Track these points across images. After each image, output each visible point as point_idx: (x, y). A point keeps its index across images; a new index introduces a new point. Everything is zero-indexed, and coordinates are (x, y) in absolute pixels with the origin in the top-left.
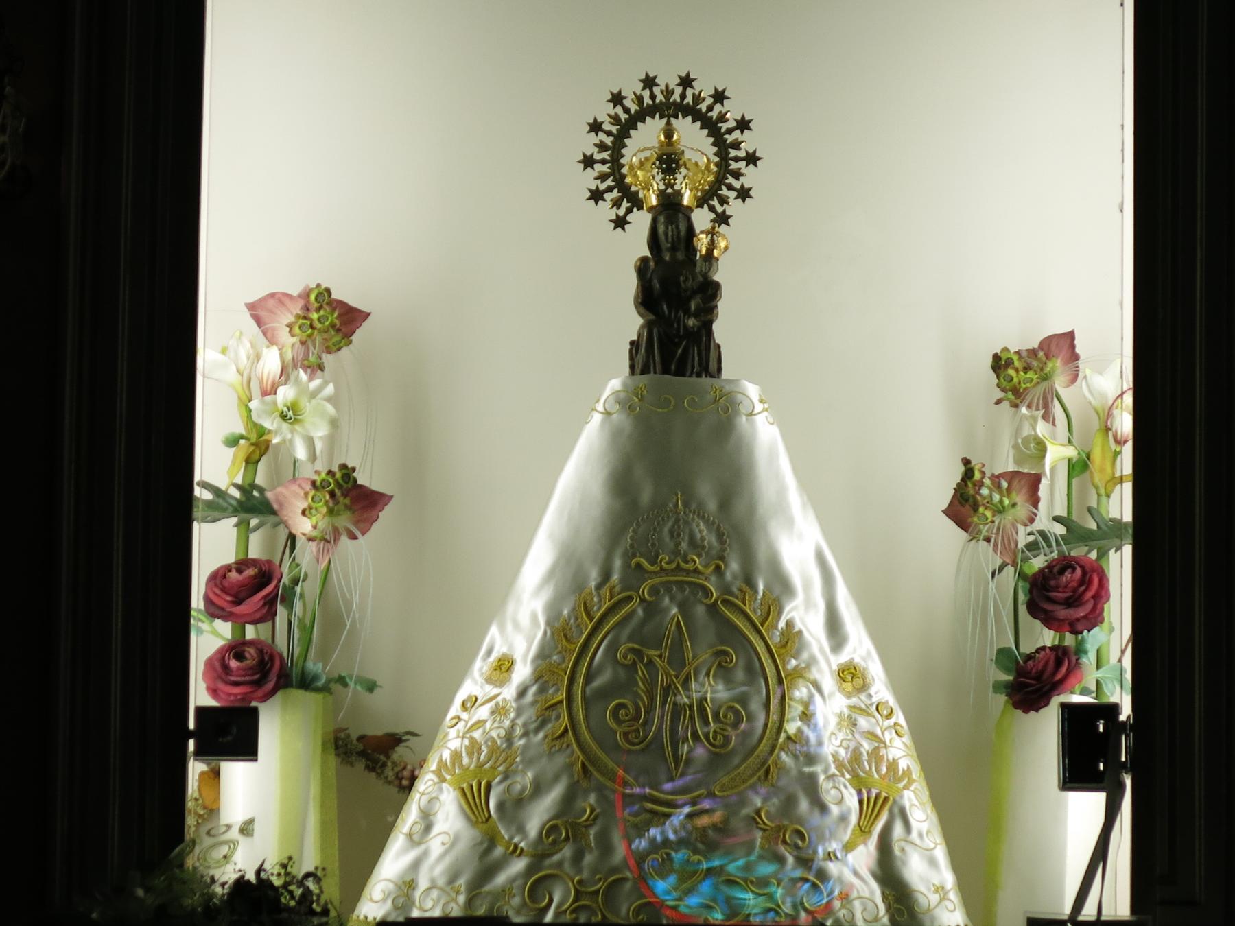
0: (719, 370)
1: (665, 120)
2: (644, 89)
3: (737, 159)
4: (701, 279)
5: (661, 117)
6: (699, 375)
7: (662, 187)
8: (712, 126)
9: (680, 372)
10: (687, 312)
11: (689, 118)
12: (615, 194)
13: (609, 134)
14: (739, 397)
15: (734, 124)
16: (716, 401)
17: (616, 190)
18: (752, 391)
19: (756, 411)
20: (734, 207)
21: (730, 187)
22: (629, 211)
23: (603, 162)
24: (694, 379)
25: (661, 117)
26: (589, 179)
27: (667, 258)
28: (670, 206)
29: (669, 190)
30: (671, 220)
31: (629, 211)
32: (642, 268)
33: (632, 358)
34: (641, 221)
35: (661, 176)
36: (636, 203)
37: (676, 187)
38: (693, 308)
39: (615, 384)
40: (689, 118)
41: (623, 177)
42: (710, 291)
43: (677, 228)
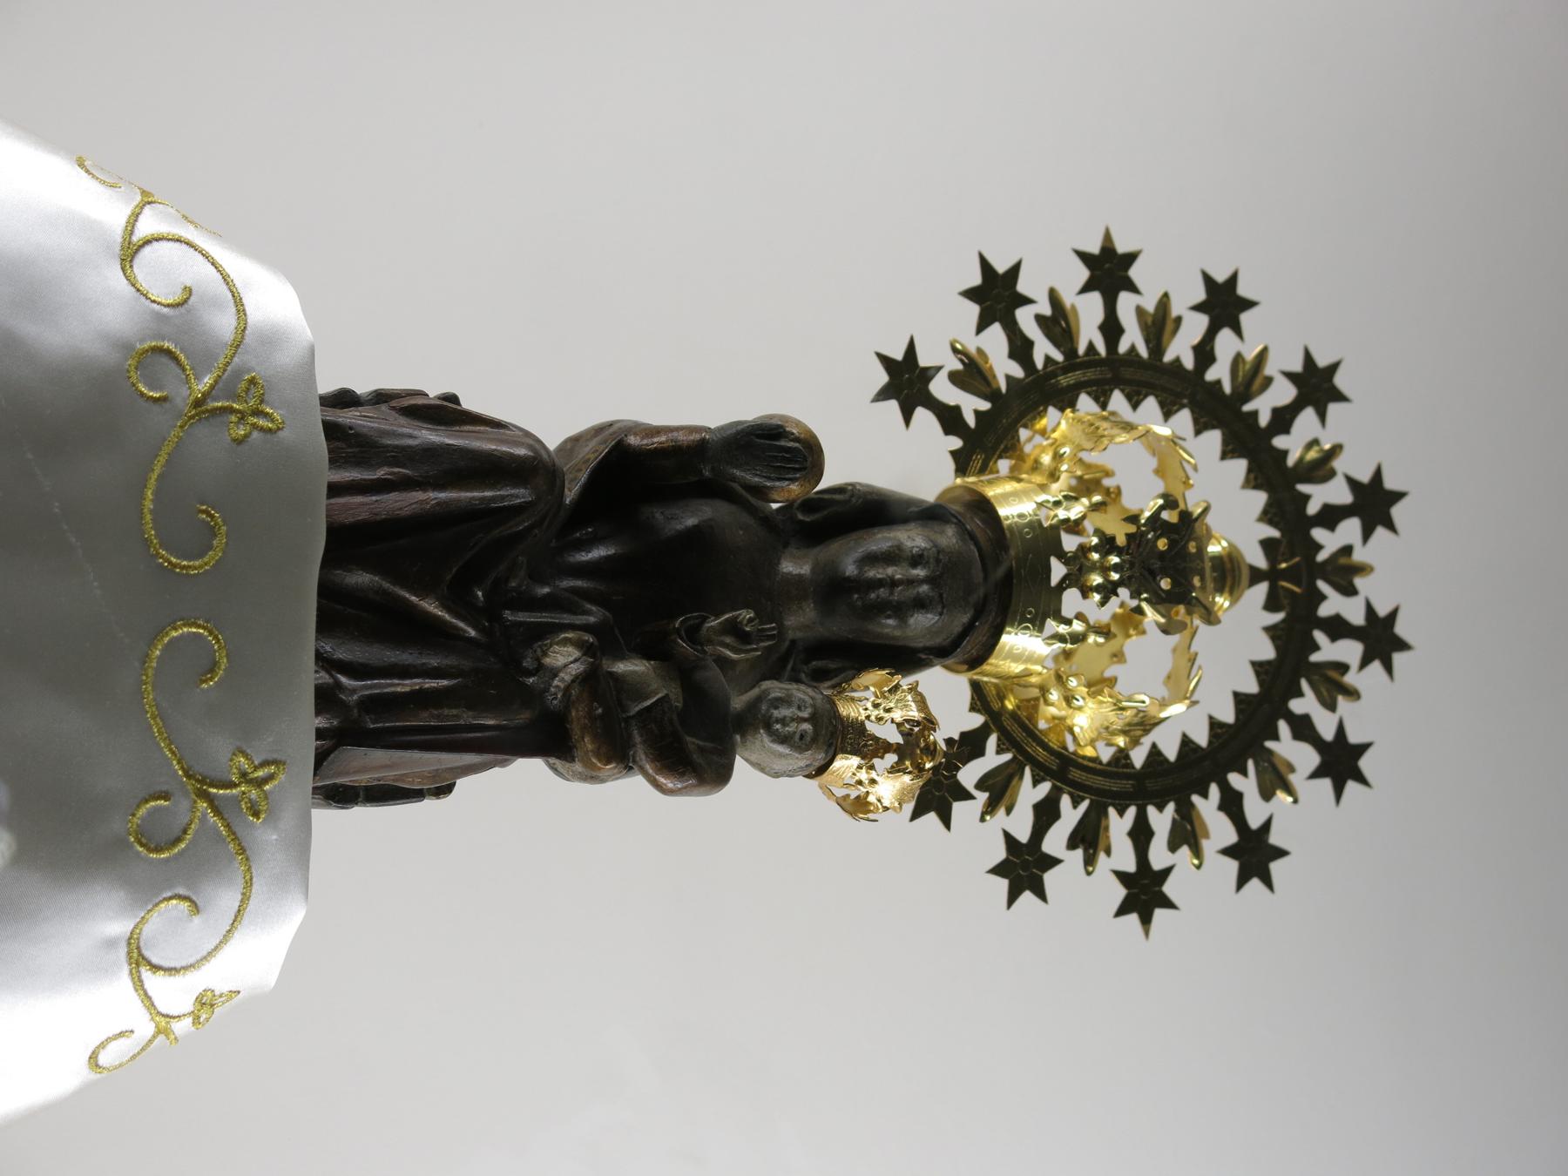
0: (340, 796)
1: (1261, 562)
2: (1353, 483)
3: (1141, 835)
4: (738, 702)
5: (1267, 545)
6: (325, 699)
7: (1070, 543)
8: (1243, 739)
9: (338, 609)
10: (602, 645)
11: (1267, 652)
13: (1204, 353)
14: (226, 899)
16: (204, 784)
18: (251, 949)
19: (152, 981)
20: (978, 835)
21: (1046, 814)
22: (950, 419)
23: (1111, 329)
24: (309, 677)
25: (1267, 545)
26: (1167, 278)
27: (788, 567)
28: (998, 577)
29: (1058, 570)
30: (946, 574)
32: (779, 448)
33: (381, 398)
34: (902, 459)
35: (1121, 533)
37: (1071, 601)
38: (621, 667)
39: (273, 301)
40: (1267, 652)
41: (1066, 401)
42: (692, 749)
43: (921, 604)
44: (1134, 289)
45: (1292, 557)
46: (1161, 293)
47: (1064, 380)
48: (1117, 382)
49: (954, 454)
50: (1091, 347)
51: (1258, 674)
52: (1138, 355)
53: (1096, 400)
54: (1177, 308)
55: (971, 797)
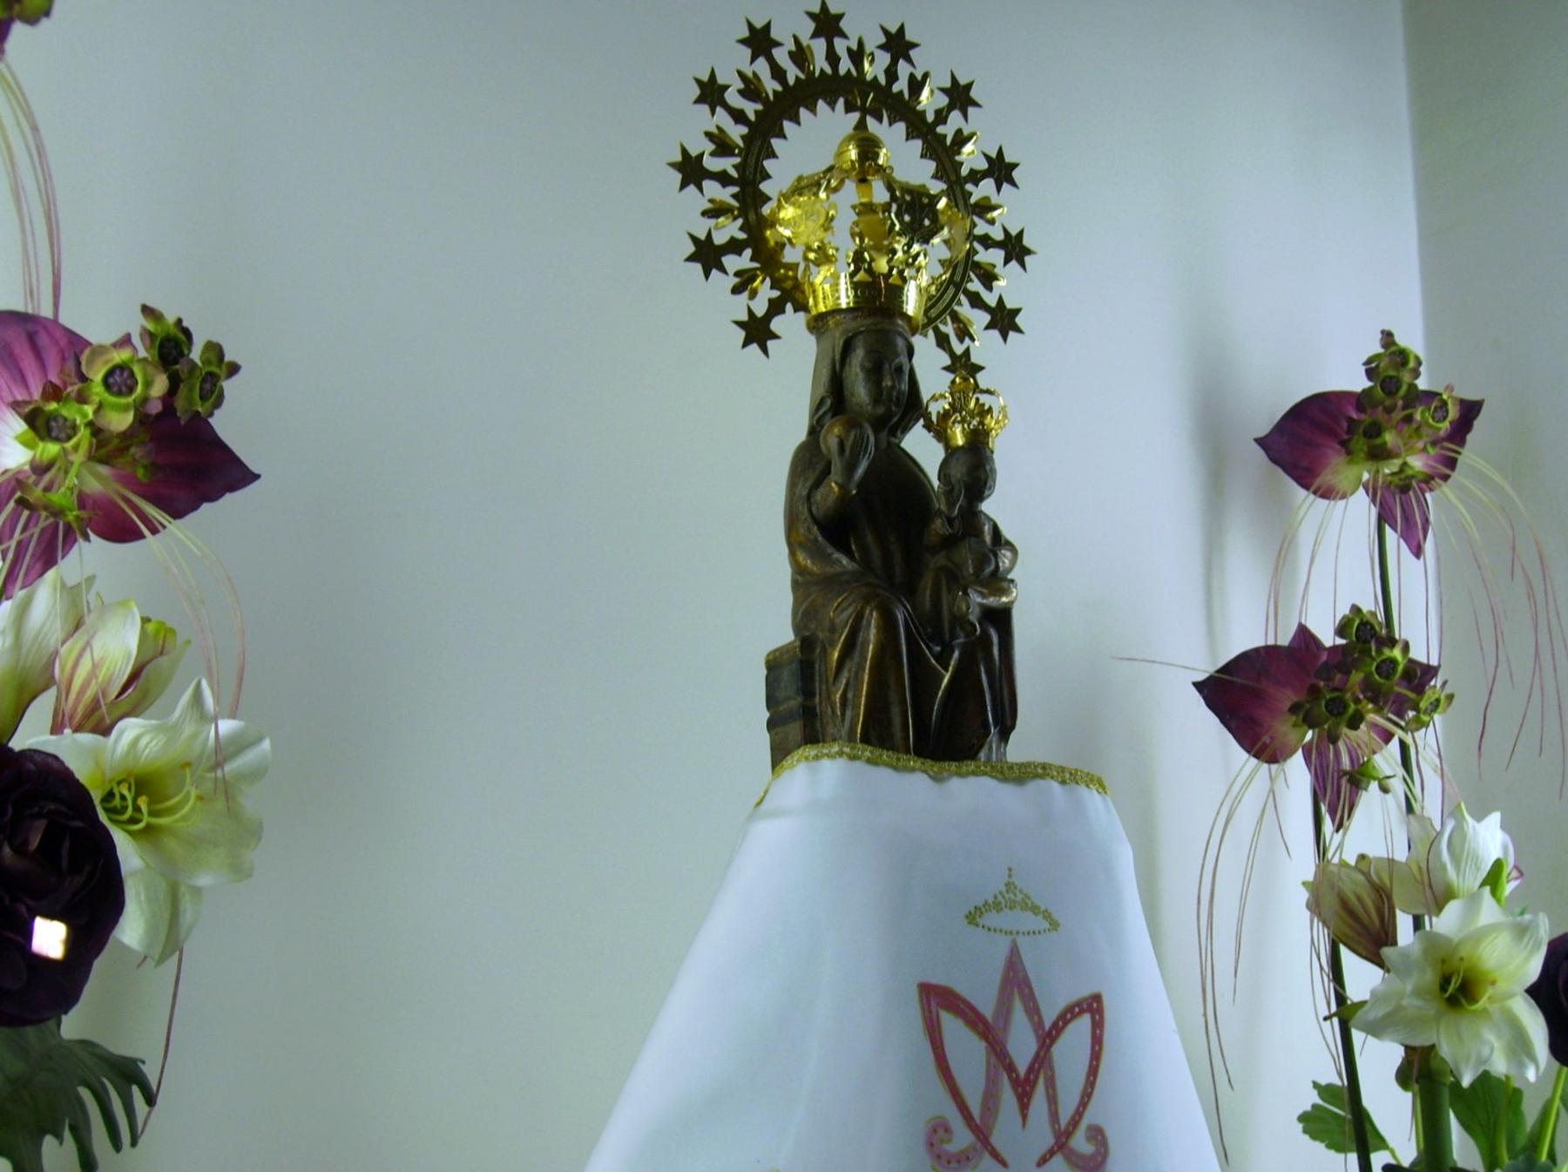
5: (849, 108)
22: (776, 308)
25: (849, 108)
31: (776, 308)
36: (792, 295)
49: (796, 310)
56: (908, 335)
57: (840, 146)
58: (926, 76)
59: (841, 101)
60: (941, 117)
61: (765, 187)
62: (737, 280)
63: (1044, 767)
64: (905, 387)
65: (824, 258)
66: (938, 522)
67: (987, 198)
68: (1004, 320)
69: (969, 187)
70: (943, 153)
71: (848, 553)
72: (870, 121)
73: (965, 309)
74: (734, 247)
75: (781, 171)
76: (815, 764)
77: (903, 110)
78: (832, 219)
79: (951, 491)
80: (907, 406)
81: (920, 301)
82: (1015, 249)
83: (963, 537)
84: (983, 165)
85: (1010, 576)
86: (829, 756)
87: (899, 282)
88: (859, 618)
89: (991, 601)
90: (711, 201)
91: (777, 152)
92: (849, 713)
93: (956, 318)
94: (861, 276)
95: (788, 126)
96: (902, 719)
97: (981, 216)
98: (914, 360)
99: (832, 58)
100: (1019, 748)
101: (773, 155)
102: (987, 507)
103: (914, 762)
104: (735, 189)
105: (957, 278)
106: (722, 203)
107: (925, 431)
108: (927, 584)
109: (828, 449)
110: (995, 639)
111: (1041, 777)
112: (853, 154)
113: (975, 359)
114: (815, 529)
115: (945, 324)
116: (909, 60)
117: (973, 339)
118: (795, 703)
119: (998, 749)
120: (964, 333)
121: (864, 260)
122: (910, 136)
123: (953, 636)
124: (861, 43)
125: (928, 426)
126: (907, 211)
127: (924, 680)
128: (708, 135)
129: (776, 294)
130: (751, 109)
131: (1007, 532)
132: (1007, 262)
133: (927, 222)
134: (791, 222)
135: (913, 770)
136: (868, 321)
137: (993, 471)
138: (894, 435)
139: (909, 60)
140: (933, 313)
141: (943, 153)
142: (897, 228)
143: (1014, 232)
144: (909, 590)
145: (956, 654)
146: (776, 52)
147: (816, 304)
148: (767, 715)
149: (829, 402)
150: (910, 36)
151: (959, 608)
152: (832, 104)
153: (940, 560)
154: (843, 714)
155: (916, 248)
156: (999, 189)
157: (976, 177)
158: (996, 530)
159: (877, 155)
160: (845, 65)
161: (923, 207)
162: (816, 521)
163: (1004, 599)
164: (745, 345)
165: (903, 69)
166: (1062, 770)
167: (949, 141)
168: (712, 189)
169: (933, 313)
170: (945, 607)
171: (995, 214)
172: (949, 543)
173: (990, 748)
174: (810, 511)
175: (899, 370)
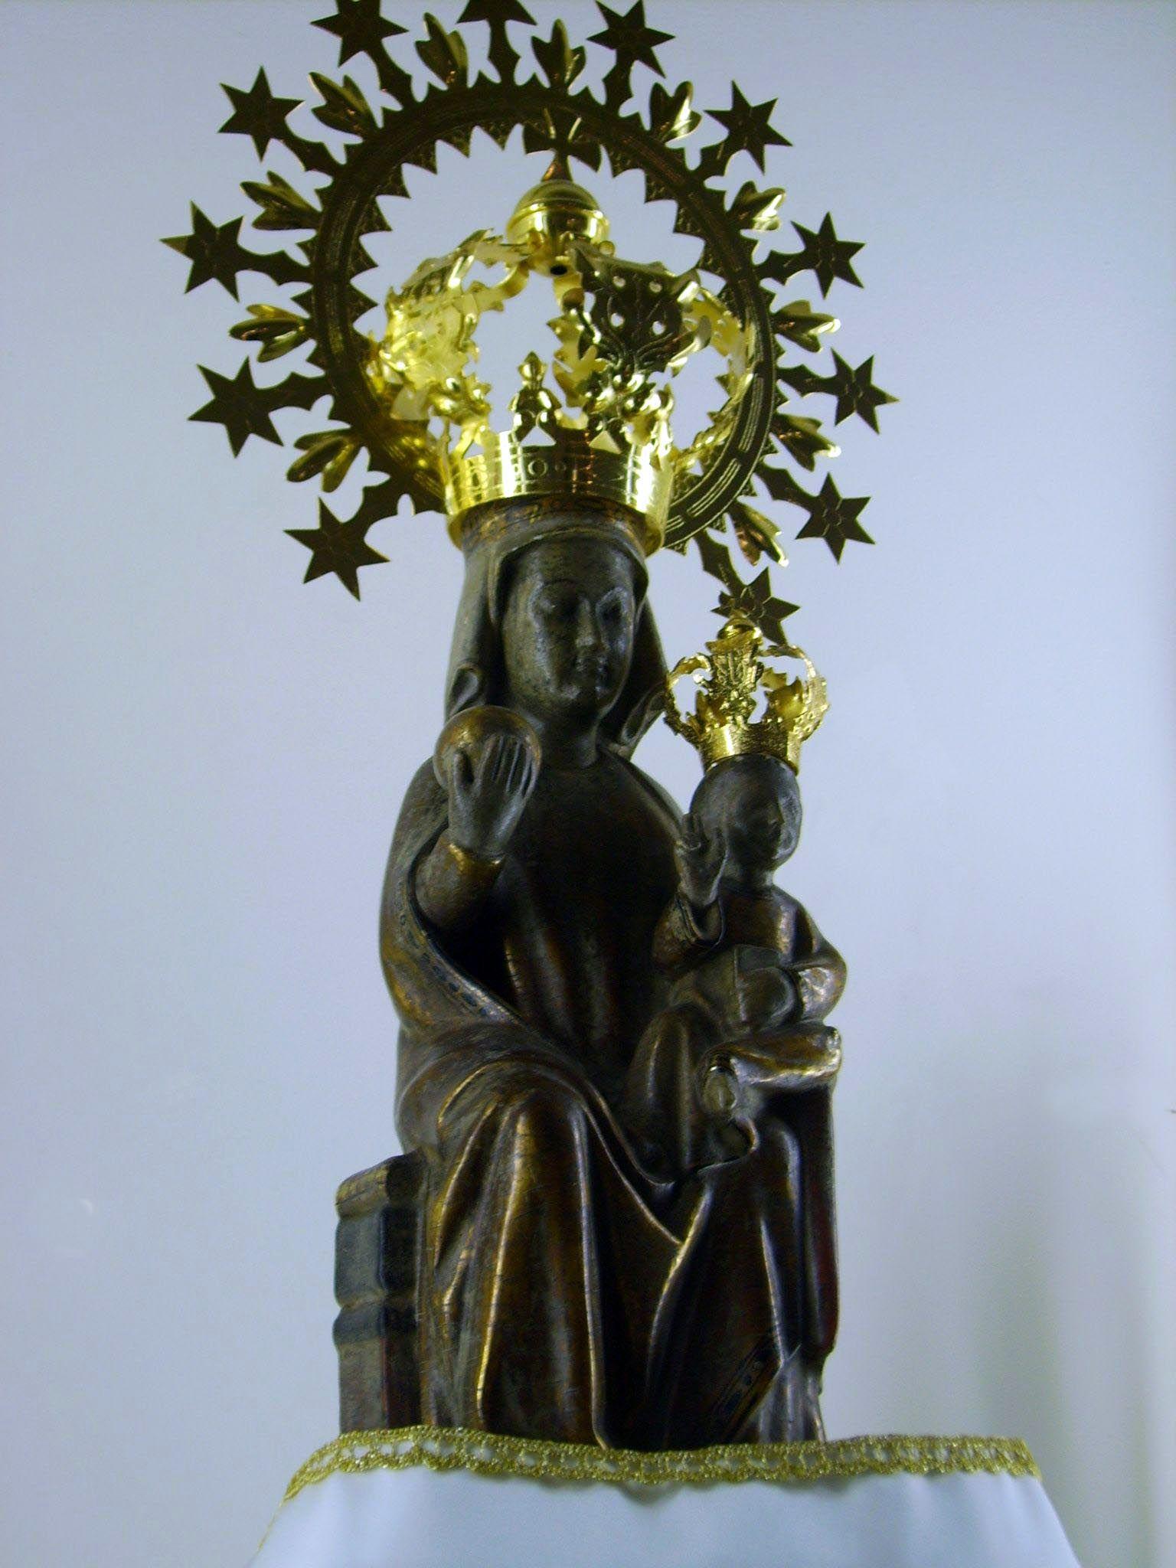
5: (533, 143)
12: (318, 418)
15: (276, 147)
17: (325, 403)
22: (378, 504)
23: (279, 268)
25: (533, 143)
26: (224, 178)
31: (378, 504)
34: (425, 572)
36: (411, 482)
41: (363, 350)
44: (292, 104)
45: (541, 115)
46: (242, 191)
47: (337, 343)
48: (342, 278)
49: (419, 510)
50: (300, 300)
51: (659, 197)
52: (312, 242)
53: (362, 311)
54: (336, 77)
55: (765, 573)
56: (638, 552)
57: (519, 207)
58: (684, 91)
59: (518, 131)
60: (714, 160)
61: (362, 283)
62: (301, 454)
63: (890, 1444)
64: (625, 644)
65: (471, 409)
66: (676, 915)
67: (803, 305)
68: (835, 520)
69: (768, 284)
70: (720, 227)
71: (499, 988)
72: (575, 165)
73: (760, 502)
74: (298, 392)
75: (390, 258)
76: (360, 1478)
77: (643, 149)
78: (472, 325)
79: (703, 851)
80: (637, 683)
81: (660, 483)
82: (857, 392)
83: (726, 946)
84: (794, 246)
85: (828, 1021)
86: (392, 1461)
87: (612, 447)
88: (490, 1129)
89: (787, 1077)
90: (252, 309)
91: (389, 217)
92: (465, 1337)
93: (744, 520)
94: (540, 438)
95: (411, 173)
96: (575, 1362)
97: (790, 335)
98: (652, 594)
99: (502, 55)
100: (848, 1395)
101: (381, 225)
102: (784, 877)
103: (601, 1459)
104: (302, 288)
105: (745, 445)
106: (281, 313)
107: (668, 731)
108: (651, 1044)
109: (444, 773)
110: (793, 1159)
111: (883, 1469)
112: (538, 220)
113: (778, 591)
114: (422, 936)
115: (721, 528)
116: (652, 63)
117: (775, 556)
118: (373, 1297)
119: (801, 1388)
120: (759, 543)
121: (538, 408)
122: (653, 194)
123: (701, 1157)
124: (558, 32)
125: (673, 722)
126: (617, 308)
127: (627, 1260)
128: (252, 190)
129: (380, 478)
130: (338, 143)
131: (827, 927)
132: (841, 415)
133: (658, 328)
134: (401, 347)
135: (586, 1481)
136: (550, 523)
137: (794, 807)
138: (615, 737)
139: (652, 63)
140: (698, 508)
141: (720, 227)
142: (597, 337)
143: (854, 364)
144: (607, 1061)
145: (705, 1200)
146: (390, 44)
147: (458, 494)
148: (334, 1310)
149: (475, 680)
150: (843, 234)
151: (712, 1100)
152: (500, 135)
153: (680, 992)
154: (456, 1338)
155: (637, 380)
156: (825, 287)
157: (780, 267)
158: (802, 924)
159: (583, 222)
160: (527, 69)
161: (650, 299)
162: (423, 920)
163: (811, 1072)
164: (312, 574)
165: (641, 78)
166: (930, 1443)
167: (728, 205)
168: (256, 287)
169: (698, 508)
170: (686, 1097)
171: (819, 331)
172: (700, 956)
173: (780, 1395)
174: (413, 901)
175: (612, 614)
